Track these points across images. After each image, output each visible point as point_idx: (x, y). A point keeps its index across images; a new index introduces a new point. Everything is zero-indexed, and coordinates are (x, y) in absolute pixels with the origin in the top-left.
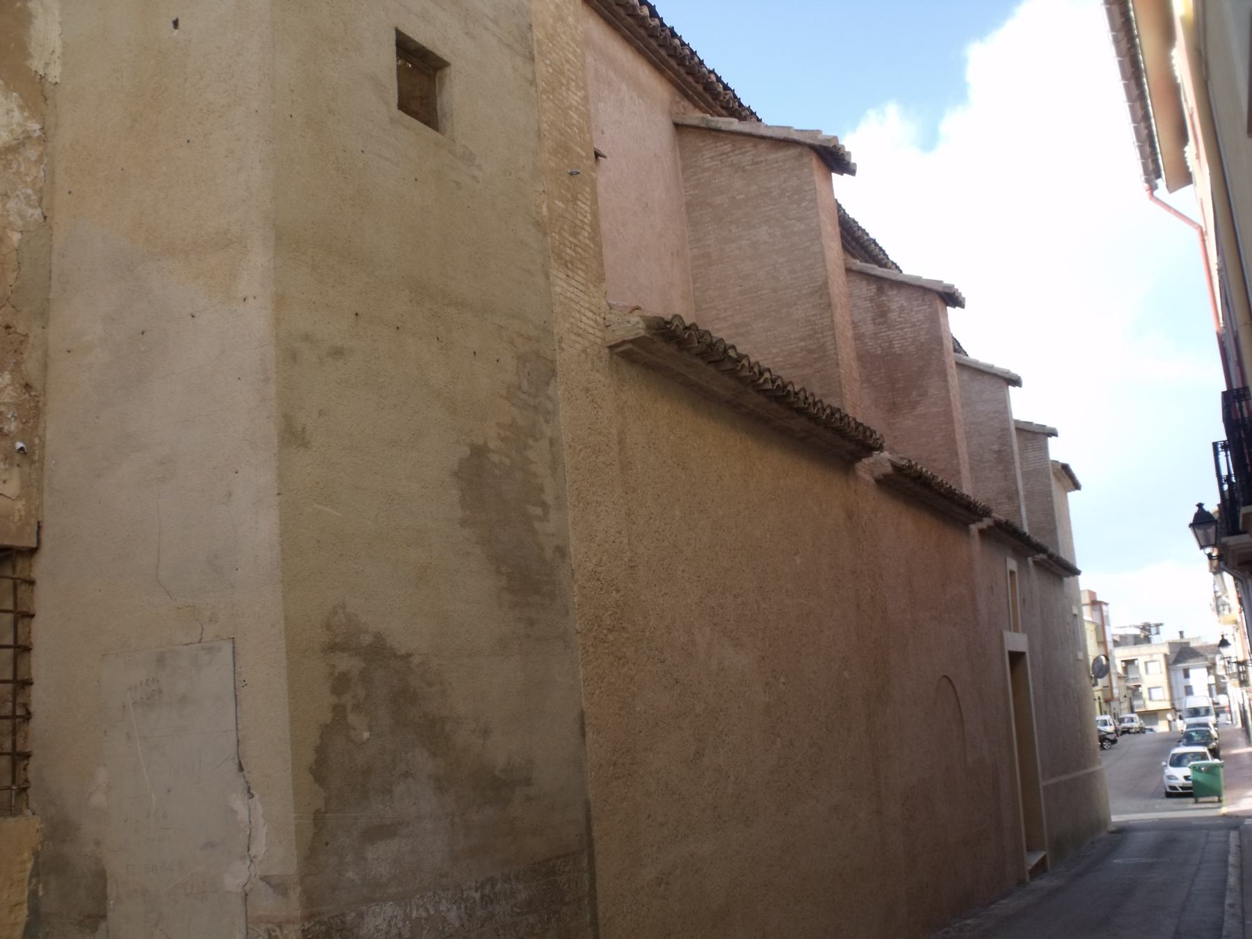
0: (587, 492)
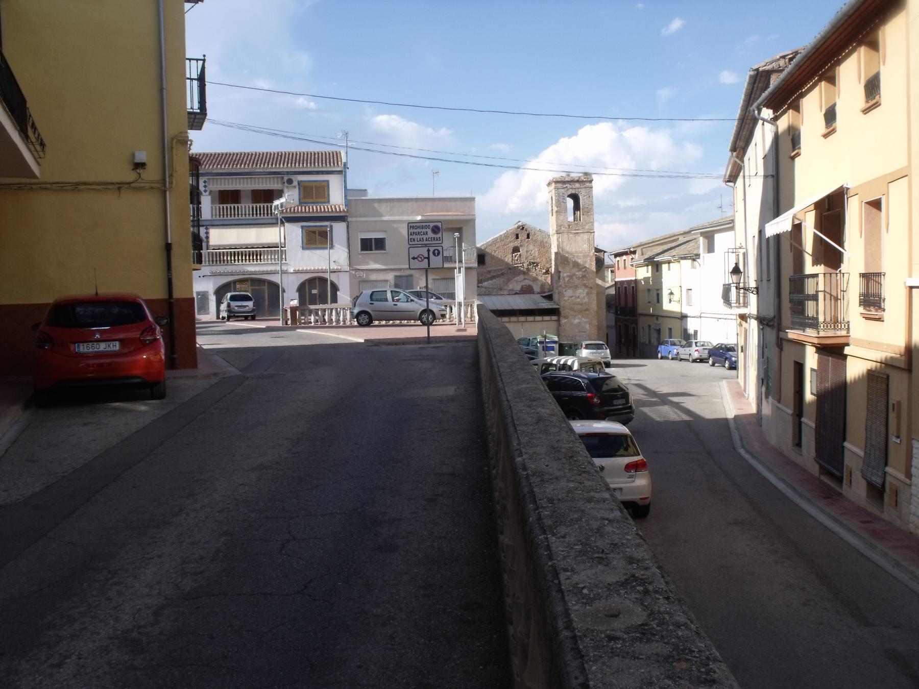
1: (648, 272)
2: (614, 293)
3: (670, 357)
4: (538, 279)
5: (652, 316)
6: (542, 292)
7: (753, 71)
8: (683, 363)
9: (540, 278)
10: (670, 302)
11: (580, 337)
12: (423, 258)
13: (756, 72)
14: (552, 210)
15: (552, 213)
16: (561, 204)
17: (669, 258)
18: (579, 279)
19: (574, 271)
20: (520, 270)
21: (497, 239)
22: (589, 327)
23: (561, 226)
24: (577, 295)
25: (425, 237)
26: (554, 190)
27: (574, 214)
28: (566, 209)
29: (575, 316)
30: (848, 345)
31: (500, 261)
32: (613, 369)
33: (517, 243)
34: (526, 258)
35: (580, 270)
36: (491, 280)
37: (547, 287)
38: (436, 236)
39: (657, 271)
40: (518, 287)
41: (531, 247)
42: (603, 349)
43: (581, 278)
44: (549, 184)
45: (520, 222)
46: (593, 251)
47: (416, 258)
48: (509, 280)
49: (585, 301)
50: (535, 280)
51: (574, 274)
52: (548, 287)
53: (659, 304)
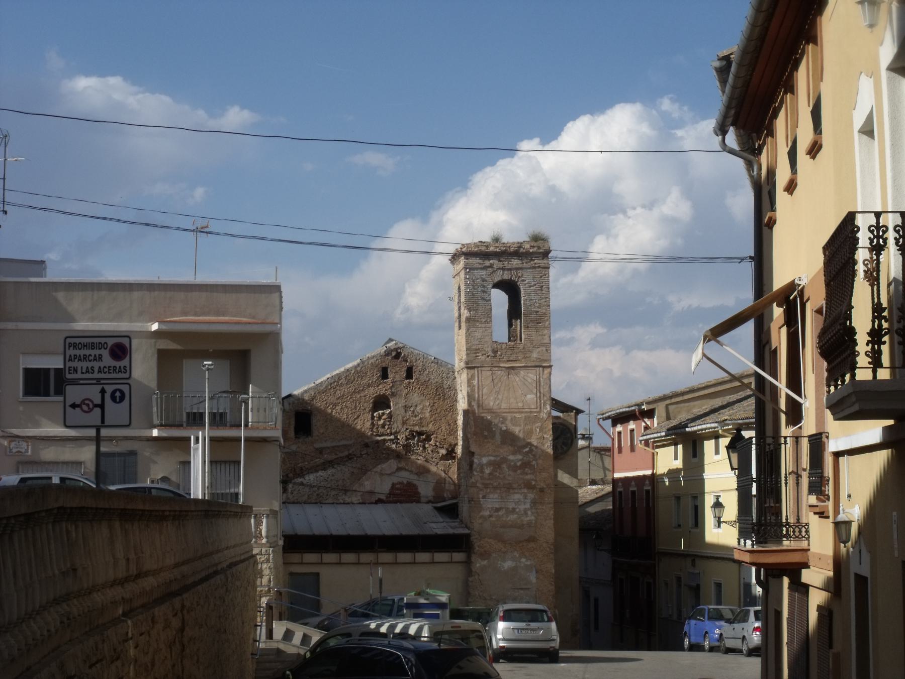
1: (676, 458)
2: (611, 507)
3: (707, 644)
4: (428, 471)
5: (683, 556)
6: (438, 498)
7: (719, 60)
8: (730, 657)
9: (433, 469)
10: (719, 526)
12: (91, 406)
13: (724, 63)
14: (460, 315)
15: (460, 322)
16: (478, 305)
17: (713, 425)
18: (515, 471)
19: (505, 451)
20: (389, 449)
21: (339, 379)
22: (537, 578)
23: (477, 351)
24: (511, 506)
25: (97, 365)
26: (463, 272)
27: (510, 325)
28: (488, 314)
30: (806, 566)
31: (345, 427)
32: (563, 665)
33: (383, 389)
34: (404, 423)
35: (518, 450)
36: (325, 469)
37: (449, 487)
38: (118, 364)
39: (695, 456)
40: (384, 487)
41: (415, 398)
42: (543, 621)
43: (520, 467)
44: (455, 258)
45: (391, 340)
46: (548, 407)
47: (78, 406)
48: (364, 471)
49: (528, 519)
50: (423, 471)
51: (505, 460)
52: (452, 487)
53: (698, 530)
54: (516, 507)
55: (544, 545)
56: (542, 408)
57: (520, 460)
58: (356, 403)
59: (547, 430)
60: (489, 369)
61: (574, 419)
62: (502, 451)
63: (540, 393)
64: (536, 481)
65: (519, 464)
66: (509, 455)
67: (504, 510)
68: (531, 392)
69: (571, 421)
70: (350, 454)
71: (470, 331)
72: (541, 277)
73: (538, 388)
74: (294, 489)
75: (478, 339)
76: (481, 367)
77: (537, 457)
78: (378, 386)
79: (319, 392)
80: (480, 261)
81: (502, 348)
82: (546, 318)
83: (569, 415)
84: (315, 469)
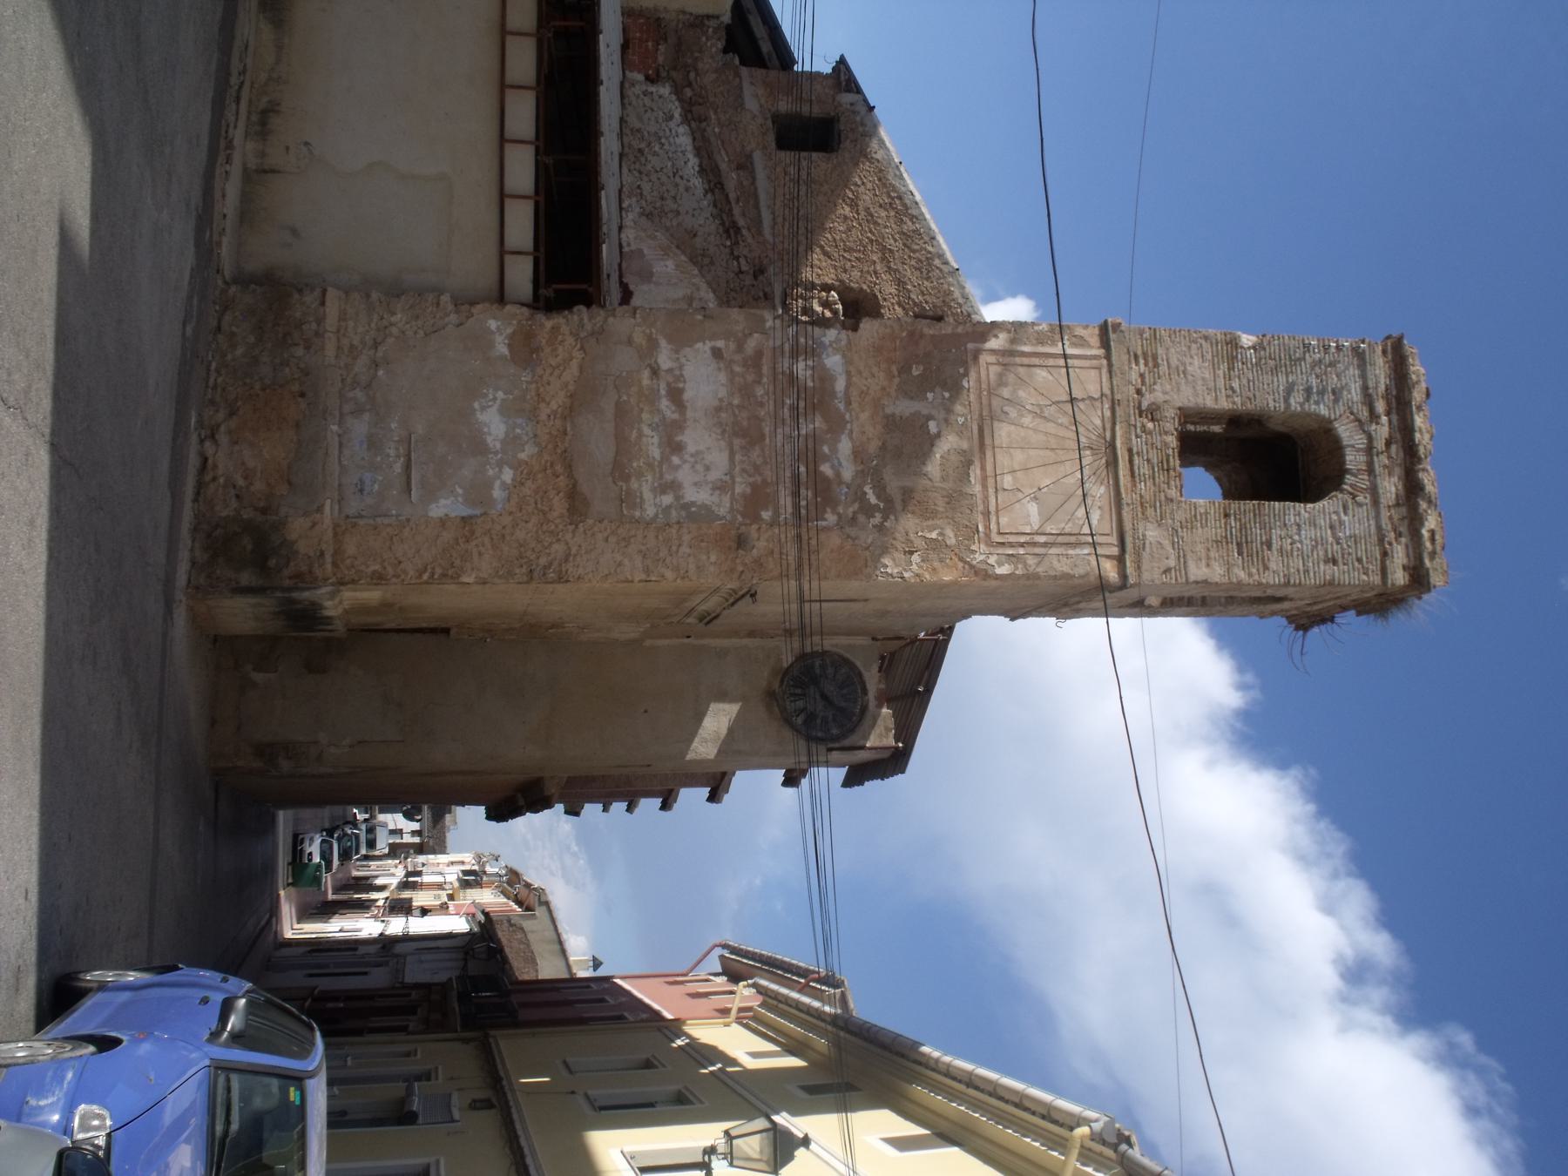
0: (738, 289)
11: (373, 444)
16: (1275, 371)
19: (863, 426)
21: (913, 218)
22: (443, 522)
23: (1153, 360)
29: (533, 416)
35: (869, 469)
36: (702, 171)
48: (700, 259)
49: (647, 495)
51: (837, 425)
54: (687, 457)
55: (558, 548)
56: (1000, 551)
57: (838, 475)
58: (859, 251)
59: (936, 564)
60: (1107, 391)
61: (877, 744)
62: (864, 416)
63: (1045, 545)
64: (774, 523)
65: (826, 469)
66: (851, 438)
67: (676, 416)
68: (1047, 518)
69: (872, 737)
70: (738, 230)
71: (1203, 342)
72: (1359, 560)
73: (1060, 539)
74: (656, 98)
75: (1184, 364)
76: (1110, 365)
77: (848, 530)
78: (899, 304)
79: (881, 171)
80: (1382, 388)
81: (1166, 433)
82: (1254, 571)
83: (888, 729)
84: (702, 148)
